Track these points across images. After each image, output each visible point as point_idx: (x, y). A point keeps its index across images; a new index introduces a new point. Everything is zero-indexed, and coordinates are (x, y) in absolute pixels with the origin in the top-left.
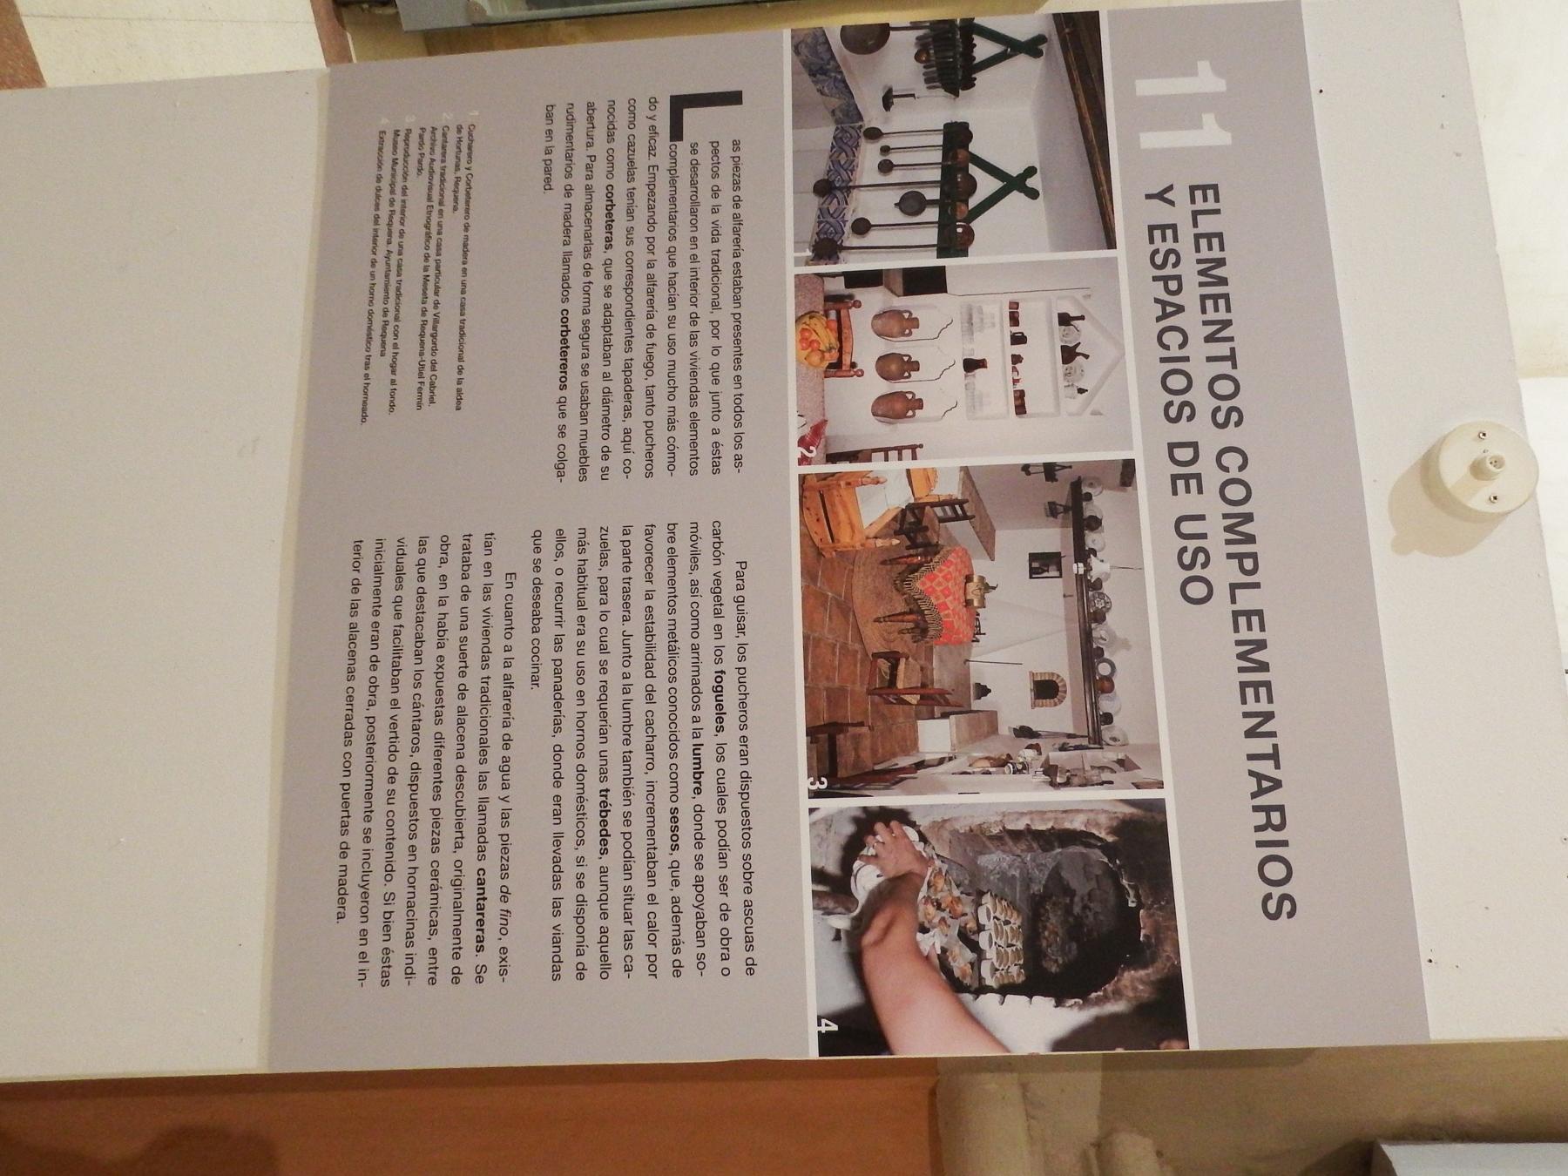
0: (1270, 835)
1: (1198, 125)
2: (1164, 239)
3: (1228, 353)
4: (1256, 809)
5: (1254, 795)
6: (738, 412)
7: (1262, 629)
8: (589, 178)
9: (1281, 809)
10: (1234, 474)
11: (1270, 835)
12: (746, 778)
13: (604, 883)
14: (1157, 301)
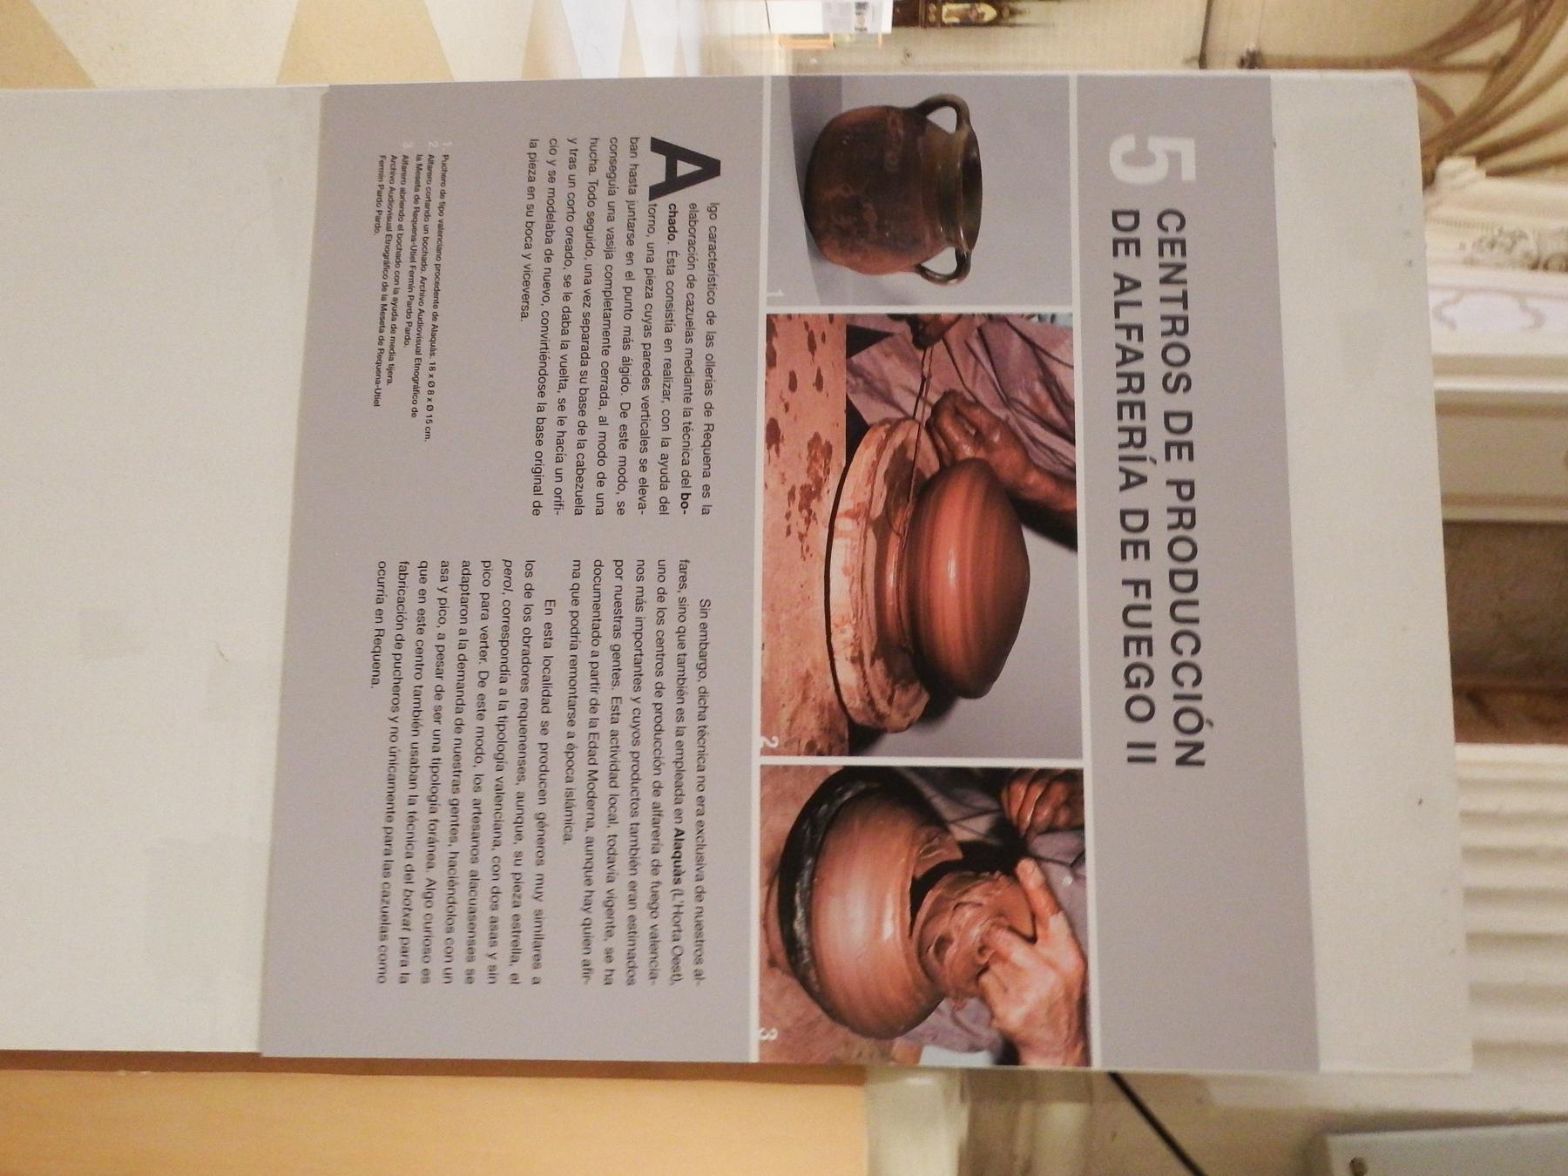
0: (1131, 451)
4: (1119, 375)
9: (1141, 376)
10: (1187, 657)
11: (1131, 451)
13: (520, 808)
14: (1118, 346)
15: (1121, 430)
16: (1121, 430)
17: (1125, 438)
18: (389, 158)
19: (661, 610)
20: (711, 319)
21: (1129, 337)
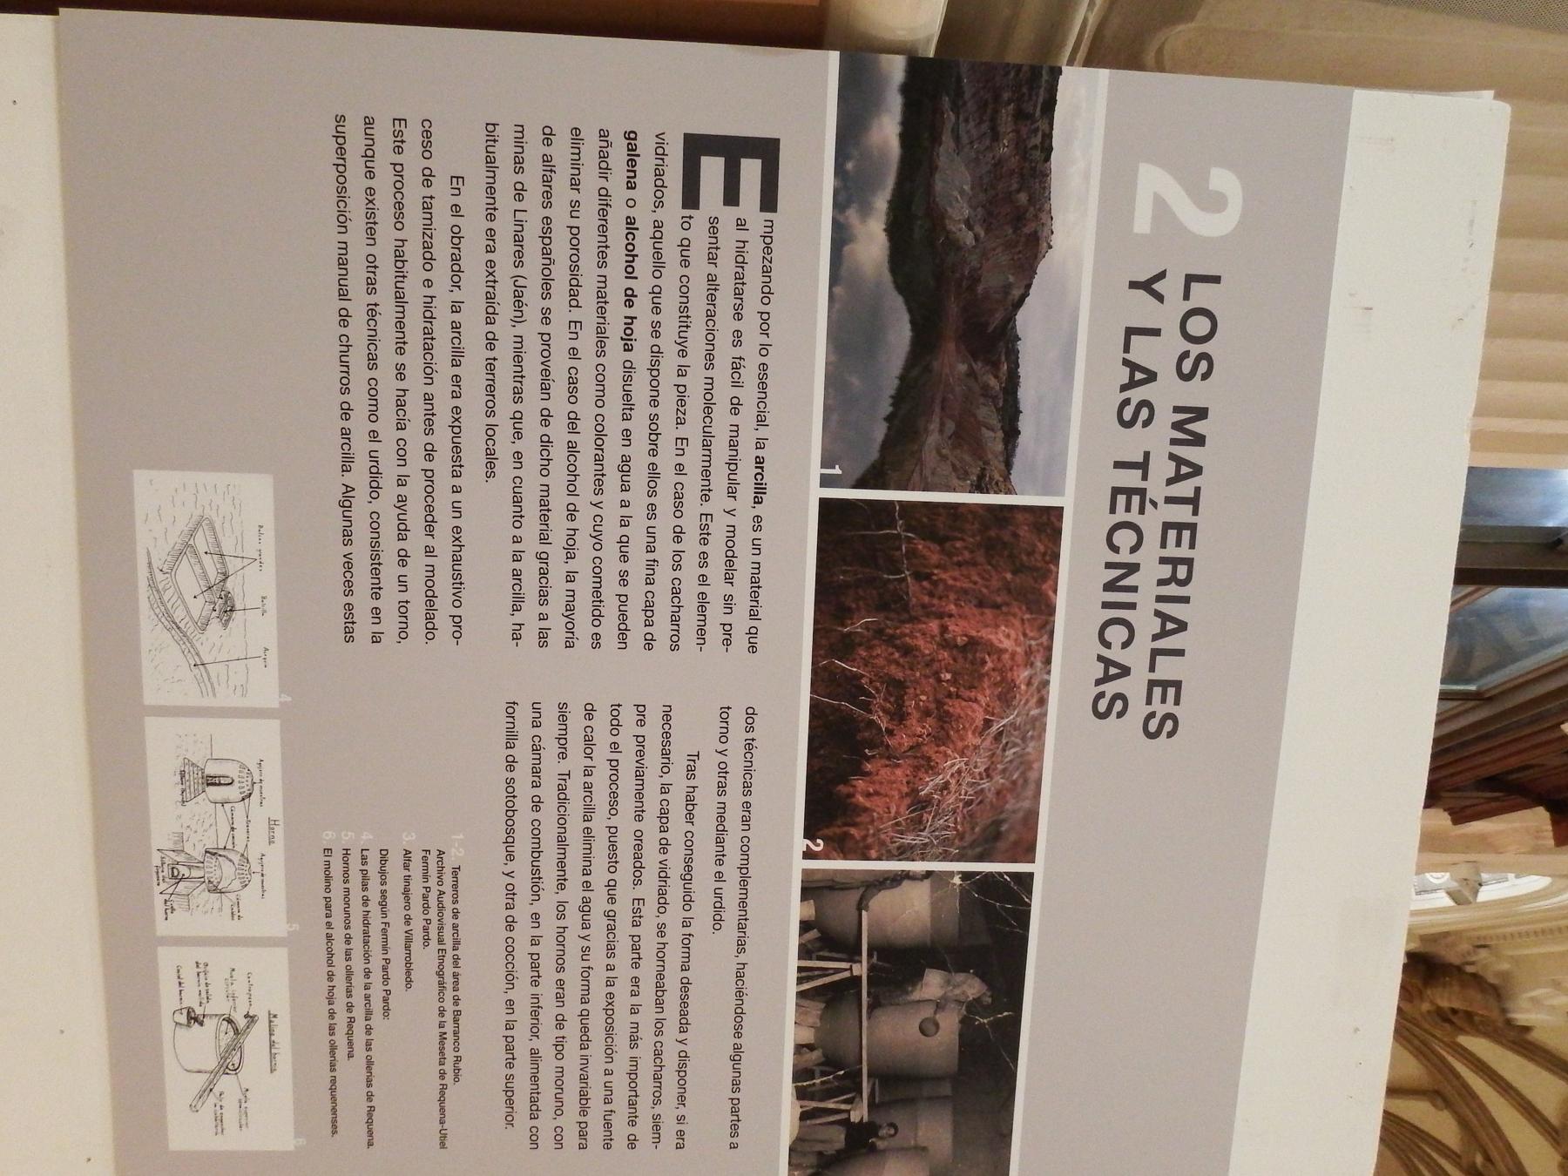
0: (1173, 590)
2: (1164, 701)
3: (1191, 494)
7: (1192, 546)
8: (536, 785)
11: (1173, 590)
12: (684, 1057)
15: (1163, 561)
16: (1163, 561)
18: (434, 853)
19: (677, 553)
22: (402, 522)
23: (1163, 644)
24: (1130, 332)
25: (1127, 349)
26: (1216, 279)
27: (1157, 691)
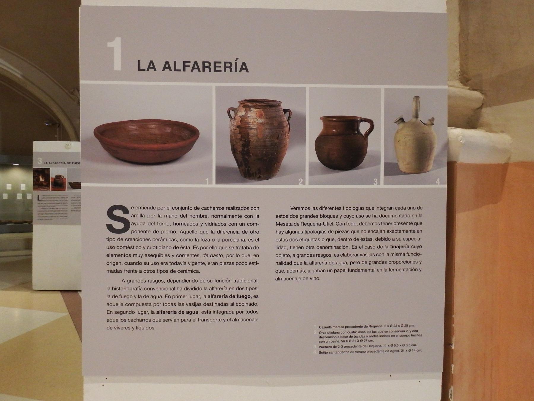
0: (233, 67)
1: (112, 50)
4: (204, 70)
5: (199, 71)
6: (339, 271)
7: (220, 63)
9: (204, 63)
11: (233, 67)
14: (192, 70)
15: (225, 71)
16: (225, 71)
17: (228, 70)
20: (197, 208)
21: (189, 66)
22: (139, 224)
23: (172, 68)
24: (139, 69)
25: (144, 70)
26: (139, 62)
27: (217, 69)
